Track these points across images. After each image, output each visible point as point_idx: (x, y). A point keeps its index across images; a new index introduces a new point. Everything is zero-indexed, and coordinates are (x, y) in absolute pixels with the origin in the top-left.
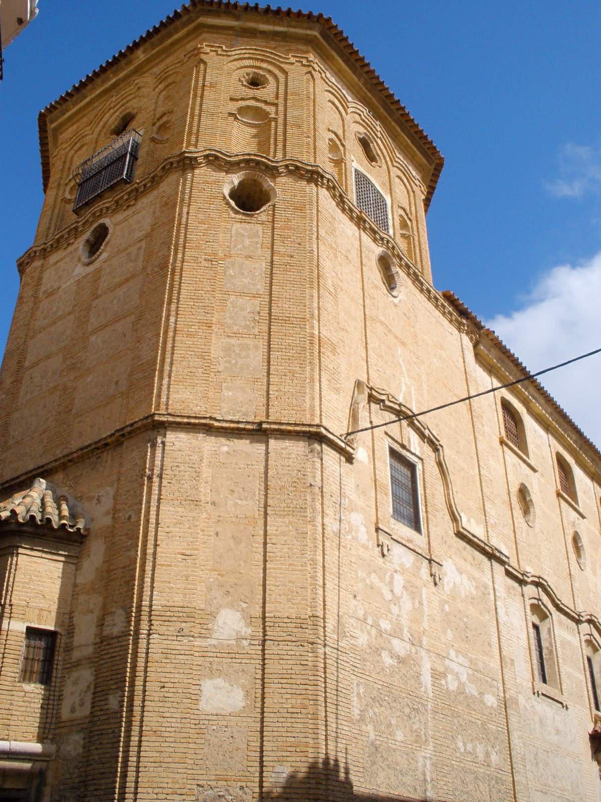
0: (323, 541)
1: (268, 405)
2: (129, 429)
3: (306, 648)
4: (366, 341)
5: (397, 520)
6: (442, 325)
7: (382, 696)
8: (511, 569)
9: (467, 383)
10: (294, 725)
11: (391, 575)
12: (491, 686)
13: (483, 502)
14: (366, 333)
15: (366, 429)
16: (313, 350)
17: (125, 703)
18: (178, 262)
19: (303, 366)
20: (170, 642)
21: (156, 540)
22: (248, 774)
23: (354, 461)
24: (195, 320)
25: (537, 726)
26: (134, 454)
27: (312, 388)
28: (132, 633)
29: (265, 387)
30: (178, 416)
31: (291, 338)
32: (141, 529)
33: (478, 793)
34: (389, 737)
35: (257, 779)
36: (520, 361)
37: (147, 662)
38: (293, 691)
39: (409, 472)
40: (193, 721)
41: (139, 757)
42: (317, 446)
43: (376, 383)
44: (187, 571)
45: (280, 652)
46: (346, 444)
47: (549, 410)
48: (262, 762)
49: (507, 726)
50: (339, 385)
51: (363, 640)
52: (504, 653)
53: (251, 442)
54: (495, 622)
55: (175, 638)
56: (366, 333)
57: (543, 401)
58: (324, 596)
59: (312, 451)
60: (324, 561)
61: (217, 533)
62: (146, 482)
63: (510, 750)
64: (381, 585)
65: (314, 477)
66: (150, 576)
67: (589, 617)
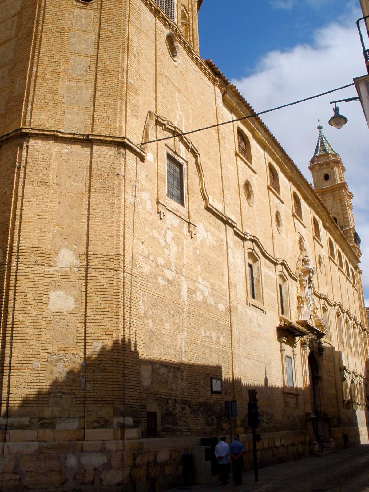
0: (125, 209)
1: (93, 124)
2: (6, 137)
3: (113, 273)
4: (156, 87)
5: (170, 198)
6: (204, 81)
7: (157, 303)
8: (237, 231)
9: (217, 117)
10: (105, 319)
11: (165, 231)
12: (222, 299)
13: (223, 190)
14: (156, 82)
15: (153, 141)
16: (122, 92)
17: (3, 306)
18: (39, 32)
19: (116, 101)
20: (30, 269)
21: (22, 206)
22: (77, 347)
23: (145, 161)
24: (49, 70)
25: (248, 322)
26: (9, 153)
27: (121, 114)
28: (7, 263)
29: (92, 113)
30: (37, 130)
31: (109, 83)
32: (13, 199)
33: (212, 359)
34: (161, 327)
35: (83, 350)
36: (250, 105)
37: (16, 281)
38: (105, 299)
39: (178, 169)
40: (44, 316)
41: (12, 337)
42: (122, 151)
43: (161, 113)
44: (41, 225)
45: (97, 275)
46: (140, 150)
47: (266, 137)
48: (85, 340)
49: (231, 322)
50: (137, 114)
51: (147, 269)
52: (231, 280)
53: (81, 147)
54: (226, 262)
55: (33, 266)
56: (156, 82)
57: (263, 131)
58: (124, 242)
59: (119, 153)
60: (124, 221)
61: (60, 202)
62: (16, 171)
63: (231, 336)
64: (159, 236)
65: (120, 169)
66: (18, 228)
67: (282, 262)
